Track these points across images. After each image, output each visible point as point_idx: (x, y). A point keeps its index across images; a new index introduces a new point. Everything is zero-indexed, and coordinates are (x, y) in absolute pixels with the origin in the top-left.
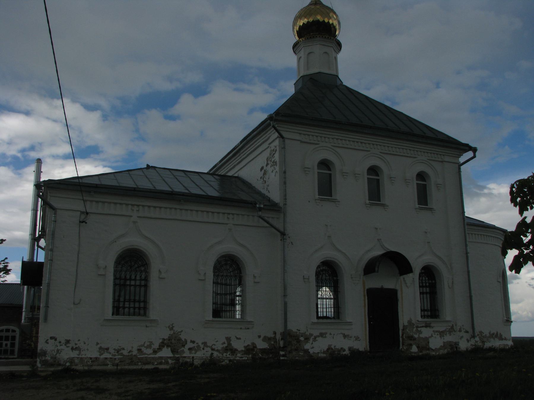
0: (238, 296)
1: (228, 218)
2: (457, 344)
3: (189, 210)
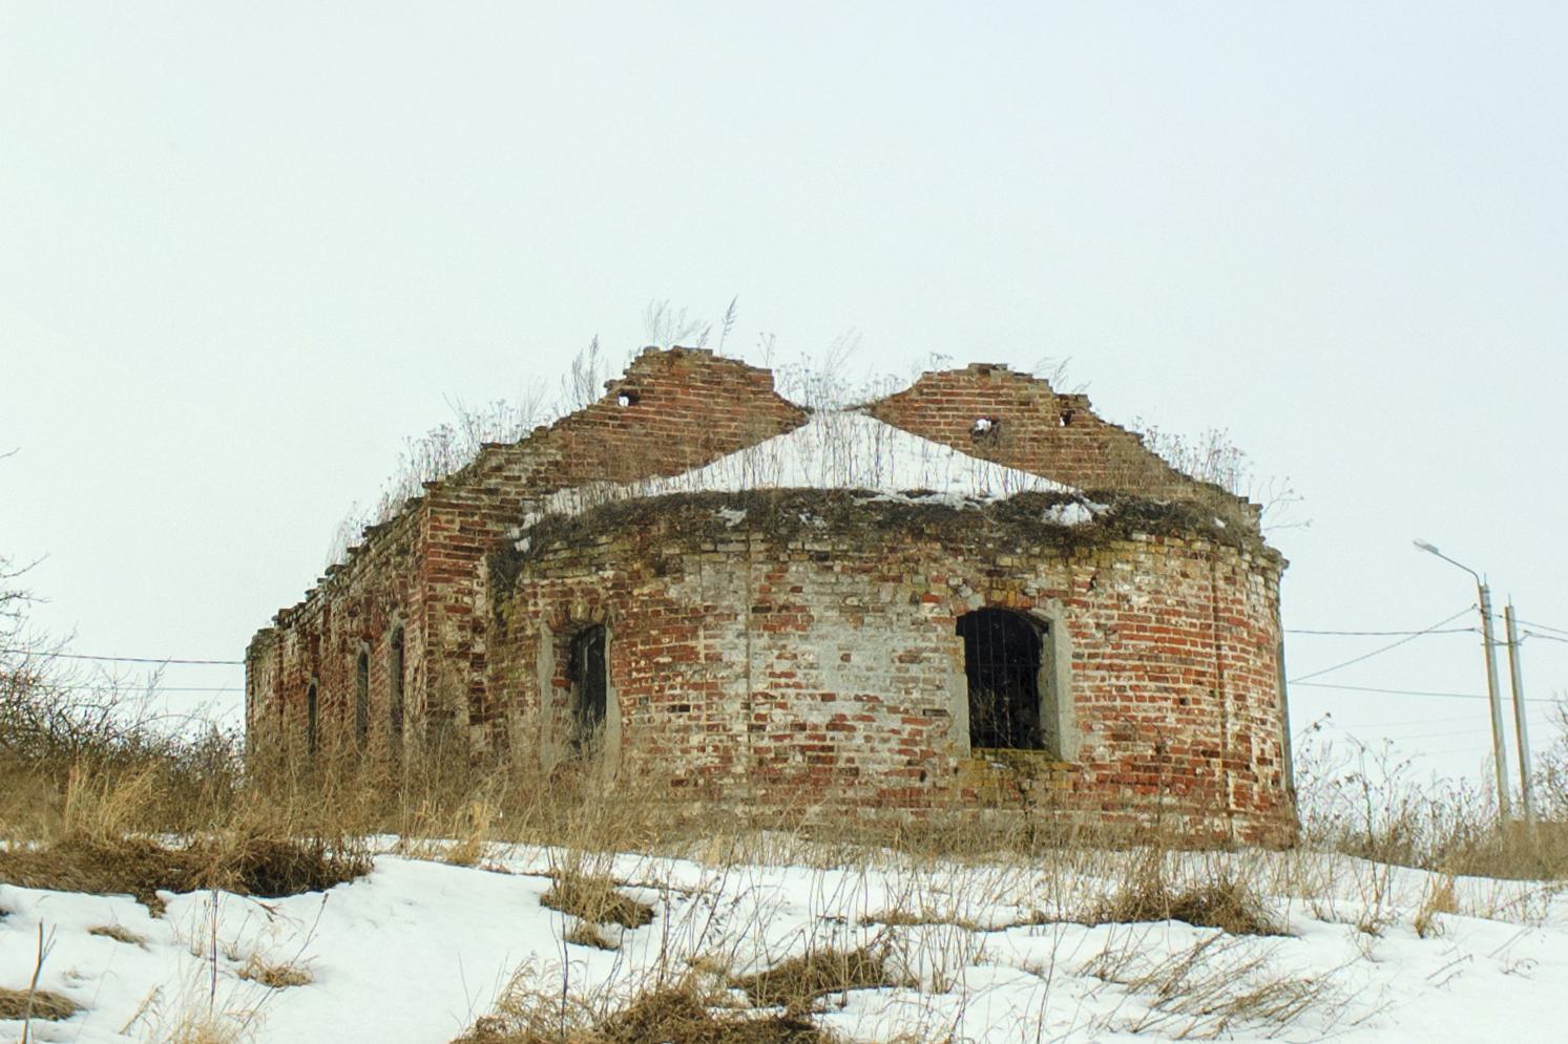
0: (803, 545)
1: (412, 640)
2: (1092, 748)
3: (1010, 926)
